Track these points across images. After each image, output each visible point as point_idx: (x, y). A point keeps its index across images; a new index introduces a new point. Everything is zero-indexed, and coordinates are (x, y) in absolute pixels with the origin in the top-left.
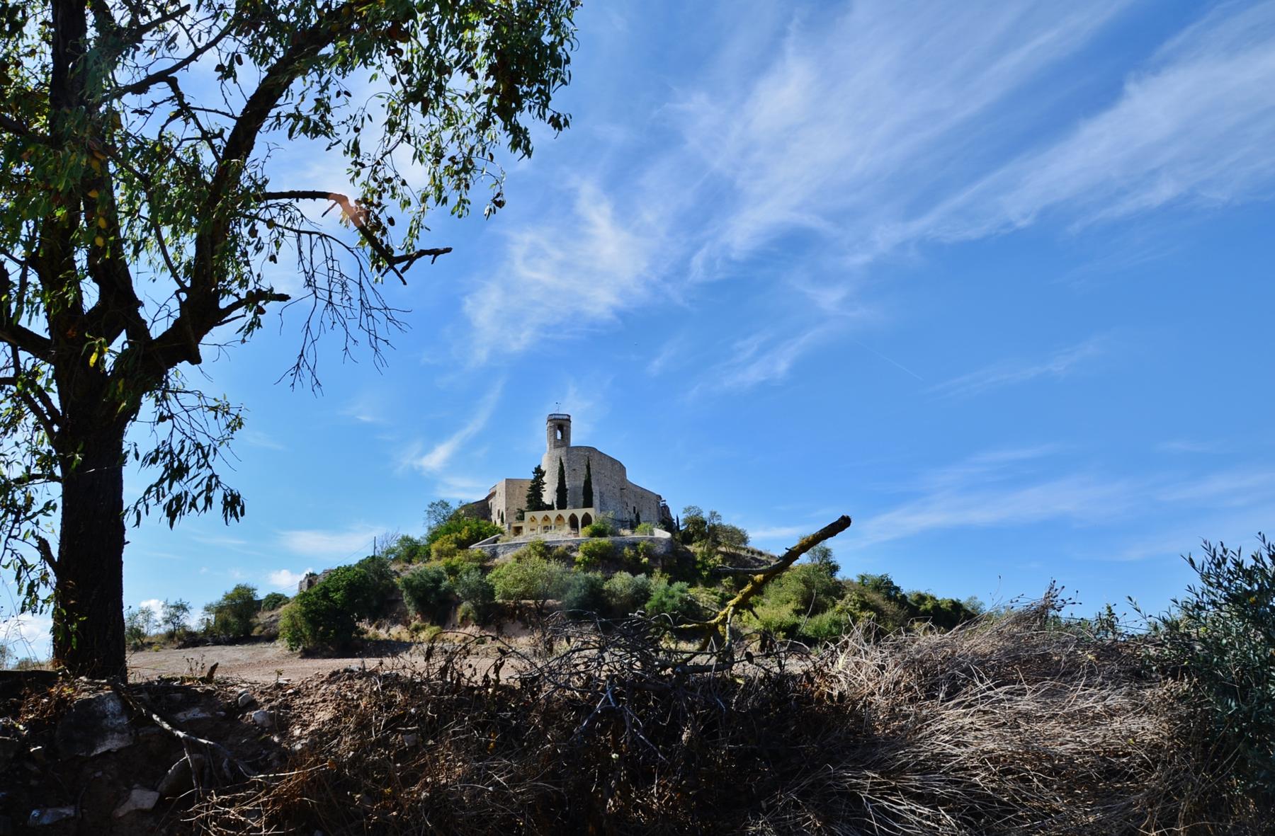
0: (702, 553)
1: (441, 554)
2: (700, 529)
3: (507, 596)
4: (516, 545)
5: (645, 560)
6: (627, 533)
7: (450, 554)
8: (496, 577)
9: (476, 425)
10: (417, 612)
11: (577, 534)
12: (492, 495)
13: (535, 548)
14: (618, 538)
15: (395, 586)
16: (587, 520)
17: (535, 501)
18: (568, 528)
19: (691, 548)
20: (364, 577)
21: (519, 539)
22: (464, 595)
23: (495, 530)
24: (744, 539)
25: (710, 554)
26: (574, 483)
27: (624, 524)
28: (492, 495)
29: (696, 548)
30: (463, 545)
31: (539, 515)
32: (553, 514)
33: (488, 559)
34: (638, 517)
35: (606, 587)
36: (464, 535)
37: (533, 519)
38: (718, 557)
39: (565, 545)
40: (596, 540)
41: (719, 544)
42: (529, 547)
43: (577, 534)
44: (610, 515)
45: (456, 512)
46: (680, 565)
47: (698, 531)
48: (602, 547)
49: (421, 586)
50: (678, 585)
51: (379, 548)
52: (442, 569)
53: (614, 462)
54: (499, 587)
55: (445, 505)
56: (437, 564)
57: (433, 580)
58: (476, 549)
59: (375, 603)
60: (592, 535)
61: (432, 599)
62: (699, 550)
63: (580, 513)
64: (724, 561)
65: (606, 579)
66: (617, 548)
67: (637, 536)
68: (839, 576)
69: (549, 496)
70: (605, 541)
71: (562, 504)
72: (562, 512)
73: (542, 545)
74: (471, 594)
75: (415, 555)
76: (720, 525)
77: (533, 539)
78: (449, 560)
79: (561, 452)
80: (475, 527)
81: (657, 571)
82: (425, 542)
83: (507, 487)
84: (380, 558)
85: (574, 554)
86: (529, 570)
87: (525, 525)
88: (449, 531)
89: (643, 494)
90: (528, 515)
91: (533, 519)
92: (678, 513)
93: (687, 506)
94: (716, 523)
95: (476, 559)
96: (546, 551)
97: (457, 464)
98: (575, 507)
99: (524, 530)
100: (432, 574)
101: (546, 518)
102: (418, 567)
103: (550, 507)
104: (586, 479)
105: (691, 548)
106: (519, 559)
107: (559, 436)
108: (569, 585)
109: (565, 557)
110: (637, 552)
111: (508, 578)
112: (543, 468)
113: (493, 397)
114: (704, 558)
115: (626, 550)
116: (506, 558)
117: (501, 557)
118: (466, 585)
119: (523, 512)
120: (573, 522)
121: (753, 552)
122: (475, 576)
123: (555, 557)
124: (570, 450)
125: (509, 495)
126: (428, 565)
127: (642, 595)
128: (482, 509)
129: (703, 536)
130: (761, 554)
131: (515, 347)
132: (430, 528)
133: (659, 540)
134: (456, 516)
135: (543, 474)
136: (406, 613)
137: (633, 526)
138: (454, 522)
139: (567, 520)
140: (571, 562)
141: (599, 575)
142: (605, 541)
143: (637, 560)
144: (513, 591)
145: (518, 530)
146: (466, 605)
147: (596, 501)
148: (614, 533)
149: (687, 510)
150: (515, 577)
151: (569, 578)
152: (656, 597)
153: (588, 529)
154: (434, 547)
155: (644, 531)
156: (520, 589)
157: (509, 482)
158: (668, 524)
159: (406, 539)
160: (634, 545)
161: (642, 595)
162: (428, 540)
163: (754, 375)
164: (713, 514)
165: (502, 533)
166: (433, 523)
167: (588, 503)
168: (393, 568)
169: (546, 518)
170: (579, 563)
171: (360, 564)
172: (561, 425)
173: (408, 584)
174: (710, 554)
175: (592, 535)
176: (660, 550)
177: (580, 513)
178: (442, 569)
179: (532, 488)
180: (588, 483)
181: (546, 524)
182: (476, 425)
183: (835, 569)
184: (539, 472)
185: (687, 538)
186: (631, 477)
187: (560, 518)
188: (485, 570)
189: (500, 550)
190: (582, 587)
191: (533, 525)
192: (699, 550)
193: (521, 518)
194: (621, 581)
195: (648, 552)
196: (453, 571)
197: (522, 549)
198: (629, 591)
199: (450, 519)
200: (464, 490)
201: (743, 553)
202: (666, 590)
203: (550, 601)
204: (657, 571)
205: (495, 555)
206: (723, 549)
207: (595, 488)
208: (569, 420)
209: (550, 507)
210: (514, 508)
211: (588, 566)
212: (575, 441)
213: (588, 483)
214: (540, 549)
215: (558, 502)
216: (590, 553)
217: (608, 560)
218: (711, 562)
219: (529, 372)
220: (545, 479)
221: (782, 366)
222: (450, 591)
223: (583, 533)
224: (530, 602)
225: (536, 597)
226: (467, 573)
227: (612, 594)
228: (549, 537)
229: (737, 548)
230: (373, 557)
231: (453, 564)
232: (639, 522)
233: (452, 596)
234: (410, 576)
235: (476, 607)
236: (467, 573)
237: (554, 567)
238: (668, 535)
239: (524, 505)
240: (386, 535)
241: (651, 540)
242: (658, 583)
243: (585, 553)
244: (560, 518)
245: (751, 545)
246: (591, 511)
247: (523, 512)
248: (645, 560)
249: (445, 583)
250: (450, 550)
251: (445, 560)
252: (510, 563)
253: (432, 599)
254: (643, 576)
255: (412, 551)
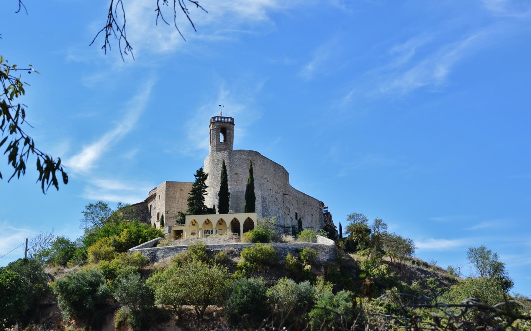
0: (367, 262)
1: (98, 257)
2: (363, 237)
3: (167, 300)
4: (177, 249)
5: (308, 267)
6: (289, 239)
7: (108, 257)
8: (156, 281)
9: (125, 126)
10: (72, 317)
11: (238, 239)
12: (152, 197)
13: (195, 252)
14: (280, 245)
15: (48, 290)
16: (249, 225)
17: (197, 205)
18: (229, 233)
19: (355, 256)
20: (16, 280)
21: (180, 243)
22: (122, 299)
23: (155, 234)
24: (409, 250)
25: (374, 264)
26: (237, 186)
27: (286, 230)
28: (152, 197)
29: (360, 257)
30: (122, 248)
31: (201, 219)
32: (214, 218)
33: (148, 263)
34: (300, 223)
35: (268, 293)
36: (123, 238)
37: (194, 223)
38: (383, 267)
39: (226, 249)
40: (258, 245)
41: (384, 253)
42: (190, 252)
43: (238, 239)
44: (273, 220)
45: (115, 214)
46: (342, 273)
47: (362, 239)
48: (264, 252)
49: (78, 291)
50: (344, 294)
51: (31, 251)
52: (100, 272)
53: (277, 166)
54: (159, 290)
55: (103, 206)
56: (93, 268)
57: (90, 284)
58: (135, 252)
59: (26, 308)
60: (254, 241)
61: (89, 303)
62: (363, 259)
63: (242, 217)
64: (389, 271)
65: (269, 286)
66: (280, 253)
67: (300, 242)
68: (512, 292)
69: (210, 200)
70: (267, 246)
71: (224, 208)
72: (224, 216)
73: (203, 249)
74: (131, 298)
75: (71, 257)
76: (386, 234)
77: (194, 243)
78: (106, 263)
79: (223, 155)
80: (135, 229)
81: (320, 280)
82: (81, 244)
83: (167, 190)
84: (33, 262)
85: (235, 259)
86: (191, 275)
87: (186, 229)
88: (107, 233)
89: (306, 200)
90: (189, 219)
91: (194, 223)
92: (341, 220)
93: (351, 213)
94: (381, 231)
95: (135, 263)
96: (207, 255)
97: (104, 166)
98: (237, 212)
99: (185, 233)
100: (88, 277)
101: (208, 222)
102: (73, 270)
103: (211, 211)
104: (244, 184)
105: (355, 256)
106: (180, 263)
107: (222, 140)
108: (231, 291)
109: (227, 262)
110: (299, 259)
111: (169, 282)
112: (205, 171)
113: (143, 98)
114: (368, 267)
115: (289, 256)
116: (166, 262)
117: (161, 260)
118: (125, 289)
119: (183, 216)
120: (235, 227)
121: (418, 264)
122: (134, 280)
123: (218, 262)
124: (233, 153)
125: (169, 198)
126: (85, 268)
127: (306, 302)
128: (142, 211)
129: (368, 245)
130: (426, 265)
131: (165, 47)
132: (87, 230)
133: (322, 248)
134: (115, 218)
135: (205, 177)
136: (60, 318)
137: (296, 232)
138: (113, 225)
139: (228, 224)
140: (233, 267)
141: (261, 281)
142: (267, 246)
143: (299, 267)
144: (173, 296)
145: (178, 234)
146: (124, 310)
147: (258, 206)
148: (276, 239)
149: (352, 217)
150: (176, 281)
151: (228, 283)
152: (320, 304)
153: (250, 234)
154: (91, 250)
155: (307, 239)
156: (182, 293)
157: (169, 184)
158: (330, 231)
159: (62, 241)
160: (297, 251)
161: (306, 302)
162: (85, 242)
163: (410, 80)
164: (378, 223)
165: (163, 236)
166: (90, 225)
167: (250, 208)
168: (47, 271)
169: (208, 222)
170: (241, 269)
171: (11, 266)
172: (223, 128)
173: (63, 287)
174: (374, 264)
175: (254, 241)
176: (323, 257)
177: (242, 217)
178: (100, 272)
179: (194, 191)
180: (250, 188)
181: (208, 228)
182: (125, 126)
183: (507, 285)
184: (201, 176)
185: (351, 247)
186: (296, 183)
187: (221, 222)
188: (145, 274)
189: (159, 254)
190: (244, 293)
191: (194, 229)
192: (363, 259)
193: (182, 222)
194: (284, 288)
195: (311, 259)
196: (110, 274)
197: (183, 253)
198: (293, 298)
199: (109, 220)
200: (113, 192)
201: (409, 264)
202: (331, 299)
203: (211, 307)
204: (320, 280)
205: (154, 258)
206: (388, 259)
207: (258, 193)
208: (232, 123)
209: (211, 211)
210: (175, 212)
211: (249, 272)
212: (238, 144)
213: (250, 188)
214: (201, 253)
215: (220, 206)
216: (252, 259)
217: (271, 266)
218: (375, 272)
219: (180, 78)
220: (207, 182)
221: (441, 72)
222: (107, 295)
223: (245, 238)
224: (191, 307)
225: (197, 303)
226: (126, 277)
227: (274, 301)
228: (210, 241)
229: (402, 258)
230: (25, 260)
231: (112, 267)
232: (301, 229)
233: (110, 301)
234: (65, 280)
235: (135, 313)
236: (126, 277)
237: (216, 271)
238: (331, 242)
239: (185, 208)
240: (40, 237)
241: (314, 247)
242: (322, 291)
243: (247, 259)
244: (221, 222)
245: (417, 255)
246: (253, 216)
247: (183, 216)
248: (308, 267)
249: (102, 287)
250: (108, 253)
251: (103, 263)
252: (171, 267)
253: (89, 303)
254: (305, 284)
255: (67, 253)
